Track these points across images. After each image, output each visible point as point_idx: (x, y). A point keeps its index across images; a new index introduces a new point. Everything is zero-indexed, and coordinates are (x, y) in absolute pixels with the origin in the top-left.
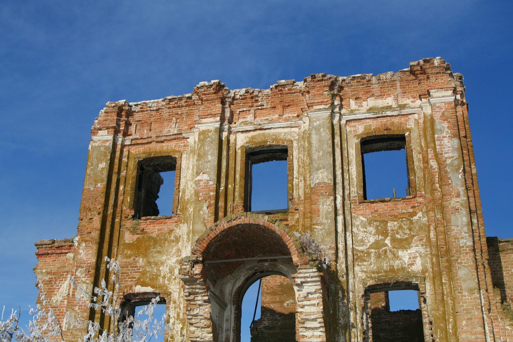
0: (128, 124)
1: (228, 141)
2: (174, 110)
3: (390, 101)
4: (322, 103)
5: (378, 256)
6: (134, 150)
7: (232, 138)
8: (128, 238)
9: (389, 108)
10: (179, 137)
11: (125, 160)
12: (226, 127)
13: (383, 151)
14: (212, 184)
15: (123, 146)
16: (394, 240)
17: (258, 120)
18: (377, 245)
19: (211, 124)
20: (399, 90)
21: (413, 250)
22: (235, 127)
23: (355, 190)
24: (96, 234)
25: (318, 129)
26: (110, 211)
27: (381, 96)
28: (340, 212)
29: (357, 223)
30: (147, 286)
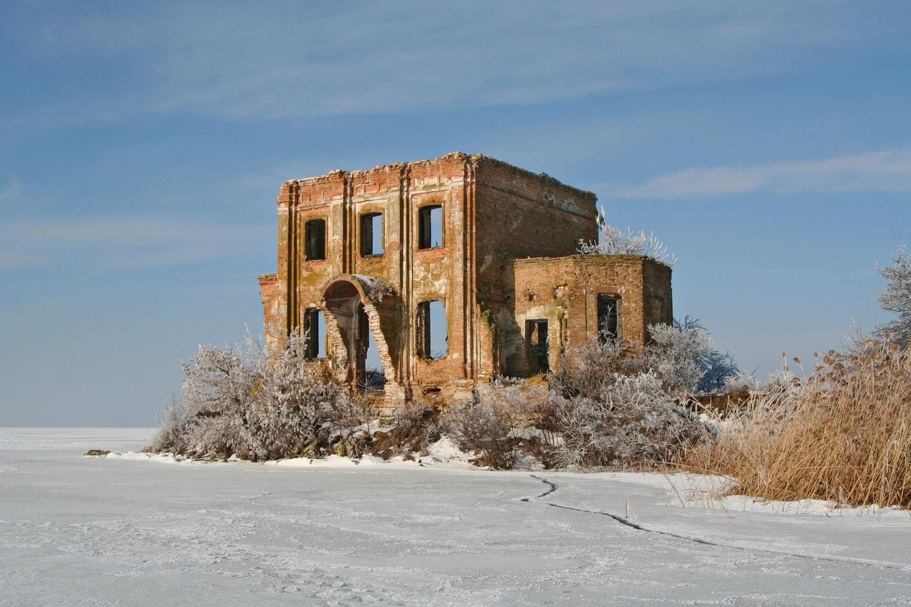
0: (297, 196)
1: (350, 209)
2: (323, 186)
3: (435, 181)
4: (395, 186)
5: (424, 285)
6: (304, 214)
7: (353, 207)
8: (305, 274)
9: (434, 186)
10: (325, 206)
11: (298, 222)
12: (348, 201)
13: (538, 172)
14: (341, 241)
15: (296, 212)
16: (432, 275)
17: (367, 195)
18: (425, 278)
19: (338, 200)
20: (441, 171)
21: (441, 281)
22: (354, 199)
23: (415, 243)
24: (286, 274)
25: (392, 204)
26: (293, 258)
27: (432, 176)
28: (405, 259)
29: (415, 264)
30: (387, 339)
